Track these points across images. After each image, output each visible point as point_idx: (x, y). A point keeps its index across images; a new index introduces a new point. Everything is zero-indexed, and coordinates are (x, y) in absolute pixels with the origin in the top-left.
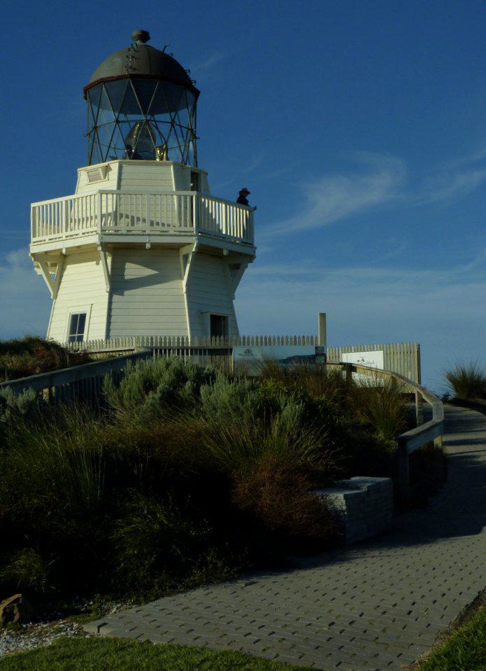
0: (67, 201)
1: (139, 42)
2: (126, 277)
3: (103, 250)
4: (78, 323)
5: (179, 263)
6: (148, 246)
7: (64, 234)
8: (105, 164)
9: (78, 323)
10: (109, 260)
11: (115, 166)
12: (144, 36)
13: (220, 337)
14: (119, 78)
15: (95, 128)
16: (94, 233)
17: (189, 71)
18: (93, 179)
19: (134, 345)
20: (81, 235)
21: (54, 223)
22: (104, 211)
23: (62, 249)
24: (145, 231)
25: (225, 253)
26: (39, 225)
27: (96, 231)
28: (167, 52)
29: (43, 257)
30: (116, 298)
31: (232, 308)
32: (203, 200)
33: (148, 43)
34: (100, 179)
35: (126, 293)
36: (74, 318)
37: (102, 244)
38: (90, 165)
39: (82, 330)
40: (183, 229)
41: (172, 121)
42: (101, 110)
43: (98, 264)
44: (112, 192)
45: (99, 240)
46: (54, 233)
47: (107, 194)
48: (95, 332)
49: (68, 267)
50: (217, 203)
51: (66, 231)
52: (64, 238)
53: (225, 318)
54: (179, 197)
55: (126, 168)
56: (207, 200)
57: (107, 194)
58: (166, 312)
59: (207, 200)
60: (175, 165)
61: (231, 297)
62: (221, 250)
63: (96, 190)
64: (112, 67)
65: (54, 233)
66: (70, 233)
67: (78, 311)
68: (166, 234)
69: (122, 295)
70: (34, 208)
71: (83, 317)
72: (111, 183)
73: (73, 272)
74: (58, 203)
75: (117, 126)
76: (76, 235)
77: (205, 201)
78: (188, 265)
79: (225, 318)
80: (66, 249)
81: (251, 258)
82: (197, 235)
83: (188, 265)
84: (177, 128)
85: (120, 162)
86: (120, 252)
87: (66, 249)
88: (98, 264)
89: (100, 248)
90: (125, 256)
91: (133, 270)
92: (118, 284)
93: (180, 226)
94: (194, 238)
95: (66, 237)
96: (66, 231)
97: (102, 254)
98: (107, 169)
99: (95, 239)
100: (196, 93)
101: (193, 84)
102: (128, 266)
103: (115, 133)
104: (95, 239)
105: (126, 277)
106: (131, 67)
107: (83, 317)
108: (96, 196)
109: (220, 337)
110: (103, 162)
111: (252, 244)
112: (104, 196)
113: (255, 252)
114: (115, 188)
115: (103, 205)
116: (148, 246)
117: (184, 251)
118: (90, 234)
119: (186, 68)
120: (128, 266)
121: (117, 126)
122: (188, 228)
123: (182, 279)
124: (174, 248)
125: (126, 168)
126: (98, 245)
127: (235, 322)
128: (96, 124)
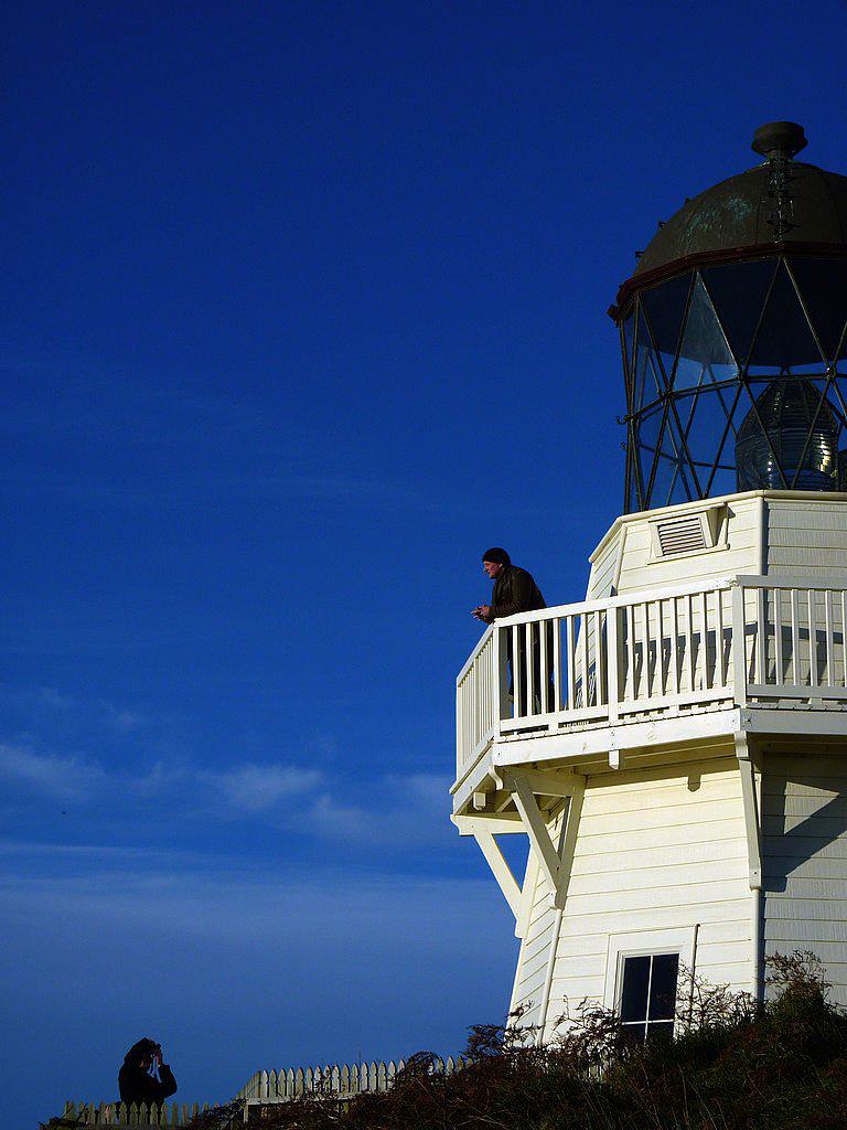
0: (536, 625)
6: (614, 761)
7: (613, 709)
8: (718, 501)
12: (791, 138)
13: (139, 1107)
14: (749, 252)
16: (729, 704)
18: (675, 544)
20: (674, 711)
23: (606, 755)
24: (805, 700)
26: (753, 659)
33: (802, 157)
34: (702, 546)
36: (635, 969)
37: (753, 739)
42: (681, 359)
45: (742, 727)
46: (523, 713)
51: (621, 698)
52: (613, 719)
65: (536, 711)
67: (650, 945)
74: (549, 623)
75: (745, 388)
76: (661, 710)
80: (622, 752)
84: (687, 468)
87: (622, 752)
89: (742, 752)
91: (803, 802)
92: (779, 851)
95: (621, 716)
96: (621, 698)
98: (722, 514)
99: (725, 723)
103: (732, 404)
106: (785, 222)
109: (139, 1107)
114: (756, 571)
116: (614, 761)
118: (640, 717)
120: (791, 788)
121: (745, 388)
126: (739, 742)
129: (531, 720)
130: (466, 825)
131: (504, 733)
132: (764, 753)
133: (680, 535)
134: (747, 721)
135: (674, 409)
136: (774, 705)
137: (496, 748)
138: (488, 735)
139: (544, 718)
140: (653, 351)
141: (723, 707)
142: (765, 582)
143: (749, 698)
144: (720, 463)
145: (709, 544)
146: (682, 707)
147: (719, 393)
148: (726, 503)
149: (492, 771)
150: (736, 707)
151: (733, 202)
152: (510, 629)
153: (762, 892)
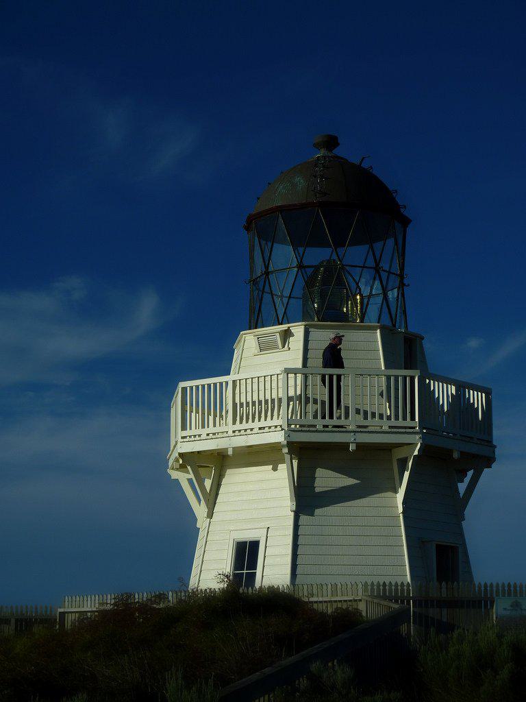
1: (322, 153)
2: (317, 490)
3: (289, 453)
4: (247, 553)
5: (392, 470)
6: (352, 447)
8: (284, 327)
9: (247, 553)
10: (295, 463)
11: (298, 330)
13: (447, 583)
15: (267, 273)
17: (396, 191)
18: (264, 347)
19: (360, 593)
20: (256, 430)
21: (213, 407)
22: (291, 393)
25: (456, 455)
27: (281, 426)
28: (365, 165)
29: (190, 460)
30: (304, 519)
31: (462, 535)
32: (427, 381)
33: (336, 151)
35: (318, 511)
37: (290, 444)
38: (256, 328)
39: (253, 564)
40: (401, 423)
41: (377, 264)
42: (275, 245)
43: (275, 469)
44: (295, 371)
45: (285, 439)
47: (295, 374)
48: (274, 571)
49: (229, 472)
50: (441, 384)
53: (453, 549)
54: (388, 378)
55: (315, 334)
56: (432, 382)
57: (295, 374)
58: (374, 547)
59: (432, 382)
60: (383, 329)
61: (460, 516)
62: (450, 452)
63: (268, 363)
64: (287, 191)
66: (238, 426)
67: (248, 536)
68: (365, 430)
69: (312, 514)
70: (184, 389)
71: (255, 545)
72: (293, 355)
73: (238, 481)
77: (430, 382)
78: (407, 474)
79: (453, 549)
81: (488, 461)
82: (421, 432)
83: (407, 474)
85: (305, 326)
86: (307, 455)
88: (275, 469)
89: (285, 450)
90: (322, 464)
91: (327, 479)
92: (307, 500)
93: (397, 418)
94: (418, 437)
95: (234, 432)
96: (234, 423)
97: (288, 457)
98: (287, 335)
99: (278, 437)
100: (405, 222)
101: (402, 210)
102: (320, 472)
104: (278, 437)
105: (317, 490)
107: (255, 545)
108: (280, 377)
110: (280, 324)
111: (491, 442)
112: (291, 376)
113: (494, 452)
114: (299, 365)
115: (293, 389)
116: (352, 447)
117: (398, 454)
119: (391, 187)
120: (320, 472)
122: (408, 423)
123: (396, 492)
124: (385, 450)
125: (315, 334)
126: (283, 446)
127: (467, 562)
128: (267, 267)
129: (244, 426)
130: (175, 475)
131: (183, 438)
132: (300, 448)
133: (267, 342)
134: (287, 436)
135: (269, 280)
136: (365, 430)
137: (179, 445)
138: (190, 437)
139: (250, 425)
140: (256, 238)
141: (270, 430)
142: (306, 370)
143: (289, 425)
144: (292, 296)
145: (280, 347)
146: (260, 429)
147: (272, 272)
148: (289, 328)
149: (177, 455)
150: (282, 430)
151: (297, 179)
152: (186, 388)
153: (297, 514)
